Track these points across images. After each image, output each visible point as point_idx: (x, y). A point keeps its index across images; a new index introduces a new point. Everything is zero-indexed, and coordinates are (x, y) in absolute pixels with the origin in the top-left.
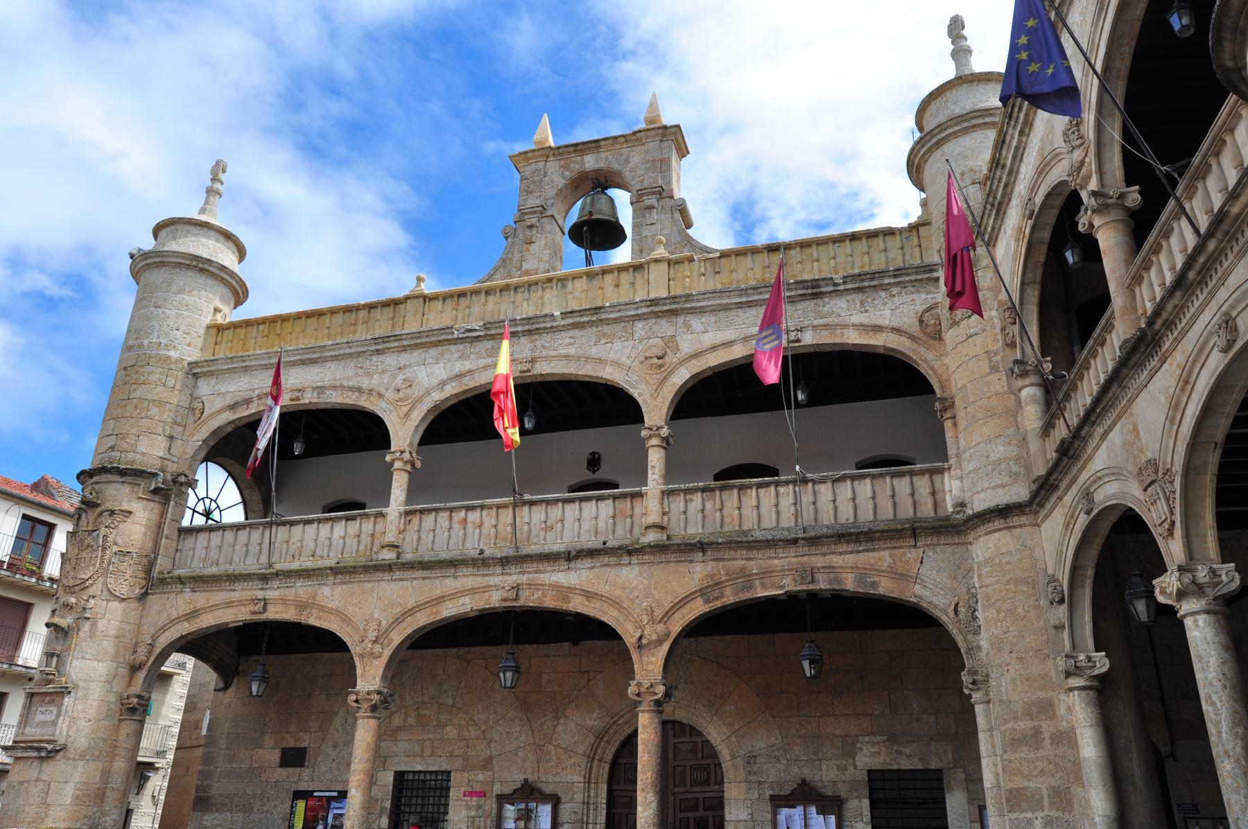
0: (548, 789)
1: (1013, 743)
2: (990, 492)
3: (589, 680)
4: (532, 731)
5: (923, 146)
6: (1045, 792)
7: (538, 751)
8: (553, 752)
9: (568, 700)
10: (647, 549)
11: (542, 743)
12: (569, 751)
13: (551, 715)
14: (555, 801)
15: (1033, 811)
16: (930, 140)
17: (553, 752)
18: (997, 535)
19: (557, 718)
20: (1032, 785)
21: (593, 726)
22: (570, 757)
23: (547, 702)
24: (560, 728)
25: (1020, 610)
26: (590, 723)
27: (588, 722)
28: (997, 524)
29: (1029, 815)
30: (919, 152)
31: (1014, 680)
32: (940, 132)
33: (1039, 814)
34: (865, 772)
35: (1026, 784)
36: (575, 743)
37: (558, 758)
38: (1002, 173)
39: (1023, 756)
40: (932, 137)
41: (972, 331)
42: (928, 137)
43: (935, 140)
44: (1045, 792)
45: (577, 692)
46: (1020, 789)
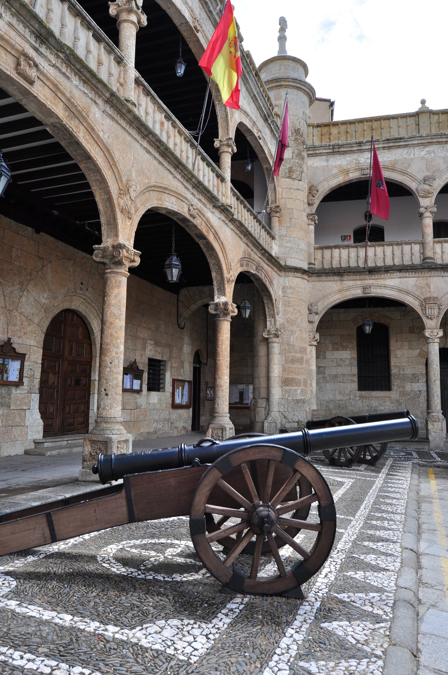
0: (20, 350)
1: (300, 361)
2: (297, 260)
3: (43, 266)
4: (4, 296)
5: (293, 82)
6: (302, 380)
7: (8, 315)
8: (19, 318)
9: (29, 277)
10: (237, 223)
11: (11, 308)
12: (30, 320)
13: (18, 286)
14: (22, 357)
15: (298, 386)
16: (298, 83)
17: (19, 318)
18: (298, 279)
19: (22, 290)
20: (299, 377)
21: (44, 303)
22: (30, 325)
23: (16, 274)
24: (23, 299)
25: (302, 312)
26: (44, 301)
27: (42, 299)
28: (299, 275)
29: (296, 388)
30: (289, 82)
31: (297, 338)
32: (303, 85)
33: (300, 388)
34: (394, 387)
35: (296, 377)
36: (33, 314)
37: (22, 324)
38: (356, 146)
39: (297, 366)
40: (299, 83)
41: (299, 188)
42: (298, 82)
43: (299, 85)
44: (302, 380)
45: (36, 273)
46: (293, 378)
